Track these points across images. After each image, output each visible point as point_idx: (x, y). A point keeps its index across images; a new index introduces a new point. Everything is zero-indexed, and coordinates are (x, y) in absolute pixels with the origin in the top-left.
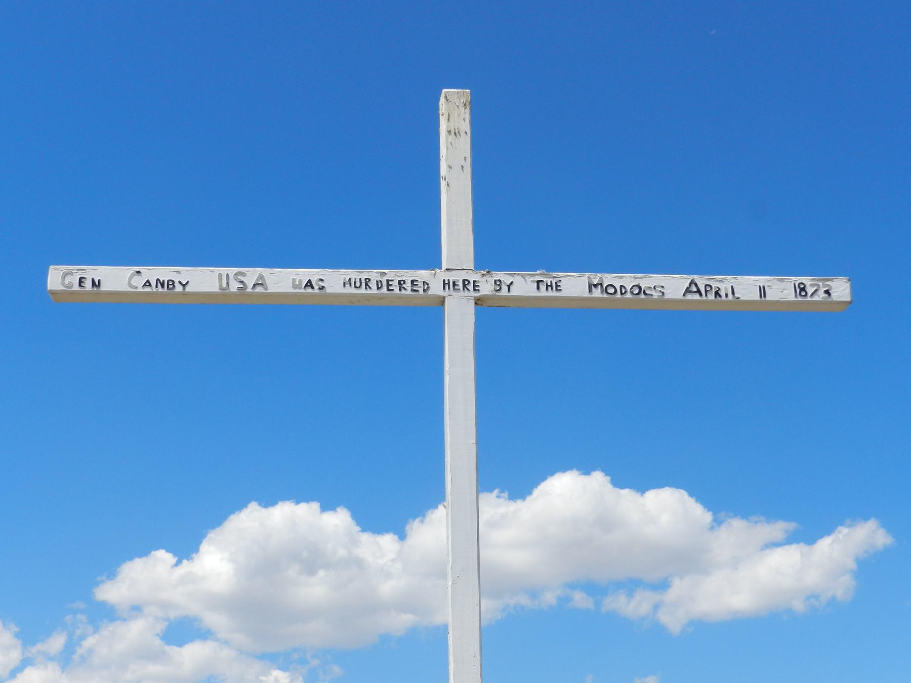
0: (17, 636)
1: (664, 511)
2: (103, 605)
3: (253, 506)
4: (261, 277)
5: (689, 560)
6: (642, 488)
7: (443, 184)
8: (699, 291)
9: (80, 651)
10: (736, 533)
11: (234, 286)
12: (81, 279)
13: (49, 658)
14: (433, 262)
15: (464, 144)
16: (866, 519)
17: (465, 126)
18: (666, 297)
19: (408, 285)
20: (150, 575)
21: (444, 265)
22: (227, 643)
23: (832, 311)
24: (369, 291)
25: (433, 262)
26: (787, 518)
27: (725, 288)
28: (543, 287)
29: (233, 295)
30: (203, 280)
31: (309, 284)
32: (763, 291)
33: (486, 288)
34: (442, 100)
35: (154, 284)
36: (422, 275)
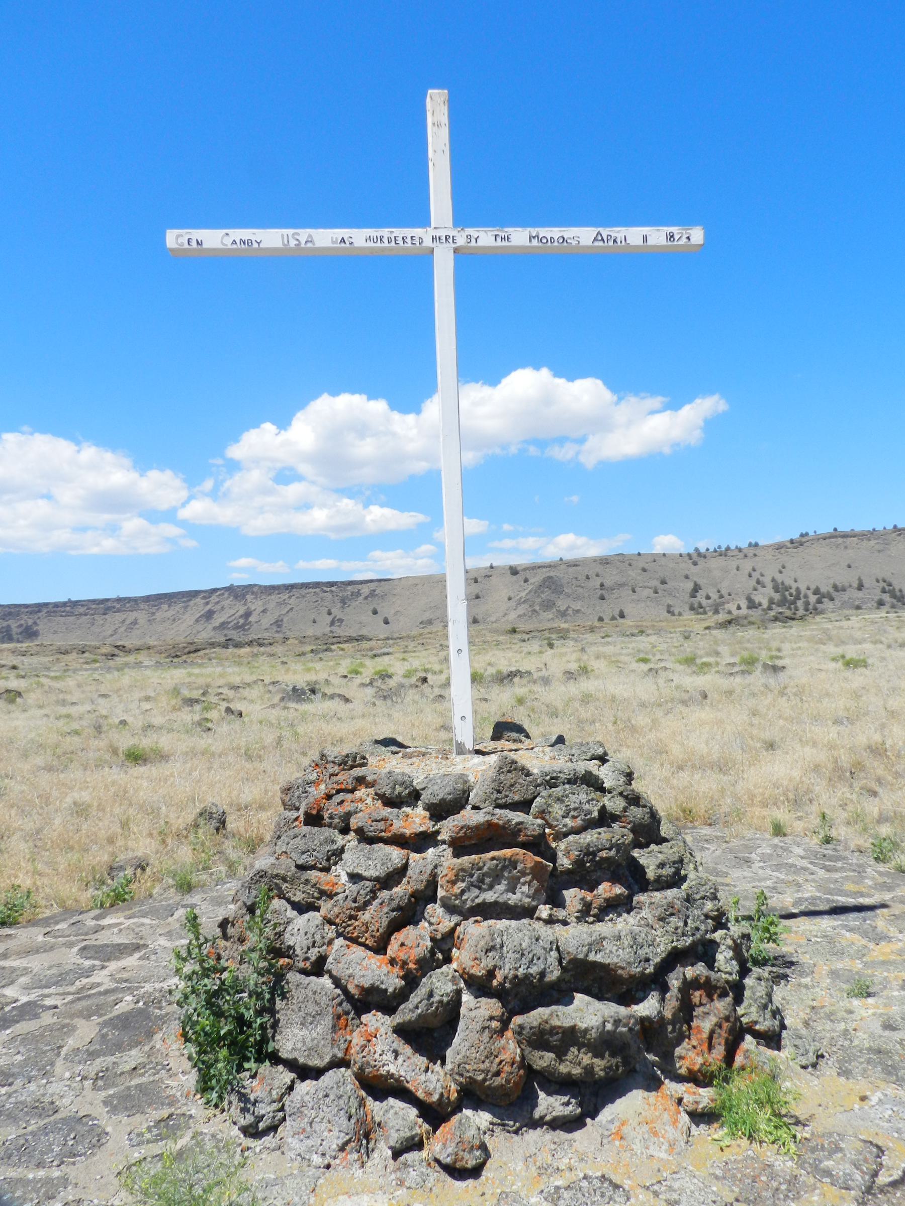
0: (185, 481)
1: (585, 393)
2: (232, 460)
3: (325, 396)
4: (310, 236)
5: (600, 424)
6: (571, 378)
7: (430, 164)
8: (603, 239)
9: (223, 489)
10: (633, 405)
11: (293, 243)
12: (189, 240)
13: (206, 495)
14: (424, 221)
15: (445, 132)
16: (712, 393)
17: (445, 119)
18: (581, 244)
19: (409, 240)
20: (260, 441)
21: (433, 225)
22: (313, 483)
23: (689, 253)
24: (383, 245)
25: (424, 221)
26: (663, 396)
27: (620, 237)
28: (499, 239)
29: (291, 249)
30: (271, 238)
31: (343, 241)
32: (645, 239)
33: (461, 241)
34: (428, 99)
35: (238, 242)
36: (418, 232)
